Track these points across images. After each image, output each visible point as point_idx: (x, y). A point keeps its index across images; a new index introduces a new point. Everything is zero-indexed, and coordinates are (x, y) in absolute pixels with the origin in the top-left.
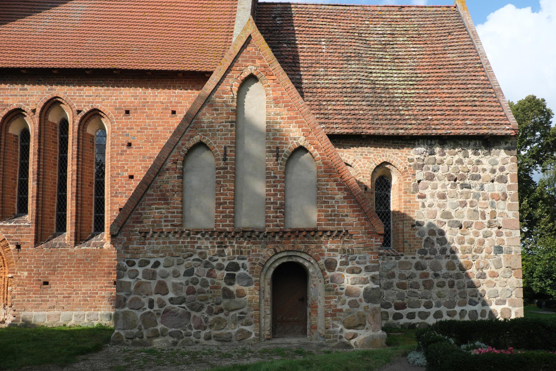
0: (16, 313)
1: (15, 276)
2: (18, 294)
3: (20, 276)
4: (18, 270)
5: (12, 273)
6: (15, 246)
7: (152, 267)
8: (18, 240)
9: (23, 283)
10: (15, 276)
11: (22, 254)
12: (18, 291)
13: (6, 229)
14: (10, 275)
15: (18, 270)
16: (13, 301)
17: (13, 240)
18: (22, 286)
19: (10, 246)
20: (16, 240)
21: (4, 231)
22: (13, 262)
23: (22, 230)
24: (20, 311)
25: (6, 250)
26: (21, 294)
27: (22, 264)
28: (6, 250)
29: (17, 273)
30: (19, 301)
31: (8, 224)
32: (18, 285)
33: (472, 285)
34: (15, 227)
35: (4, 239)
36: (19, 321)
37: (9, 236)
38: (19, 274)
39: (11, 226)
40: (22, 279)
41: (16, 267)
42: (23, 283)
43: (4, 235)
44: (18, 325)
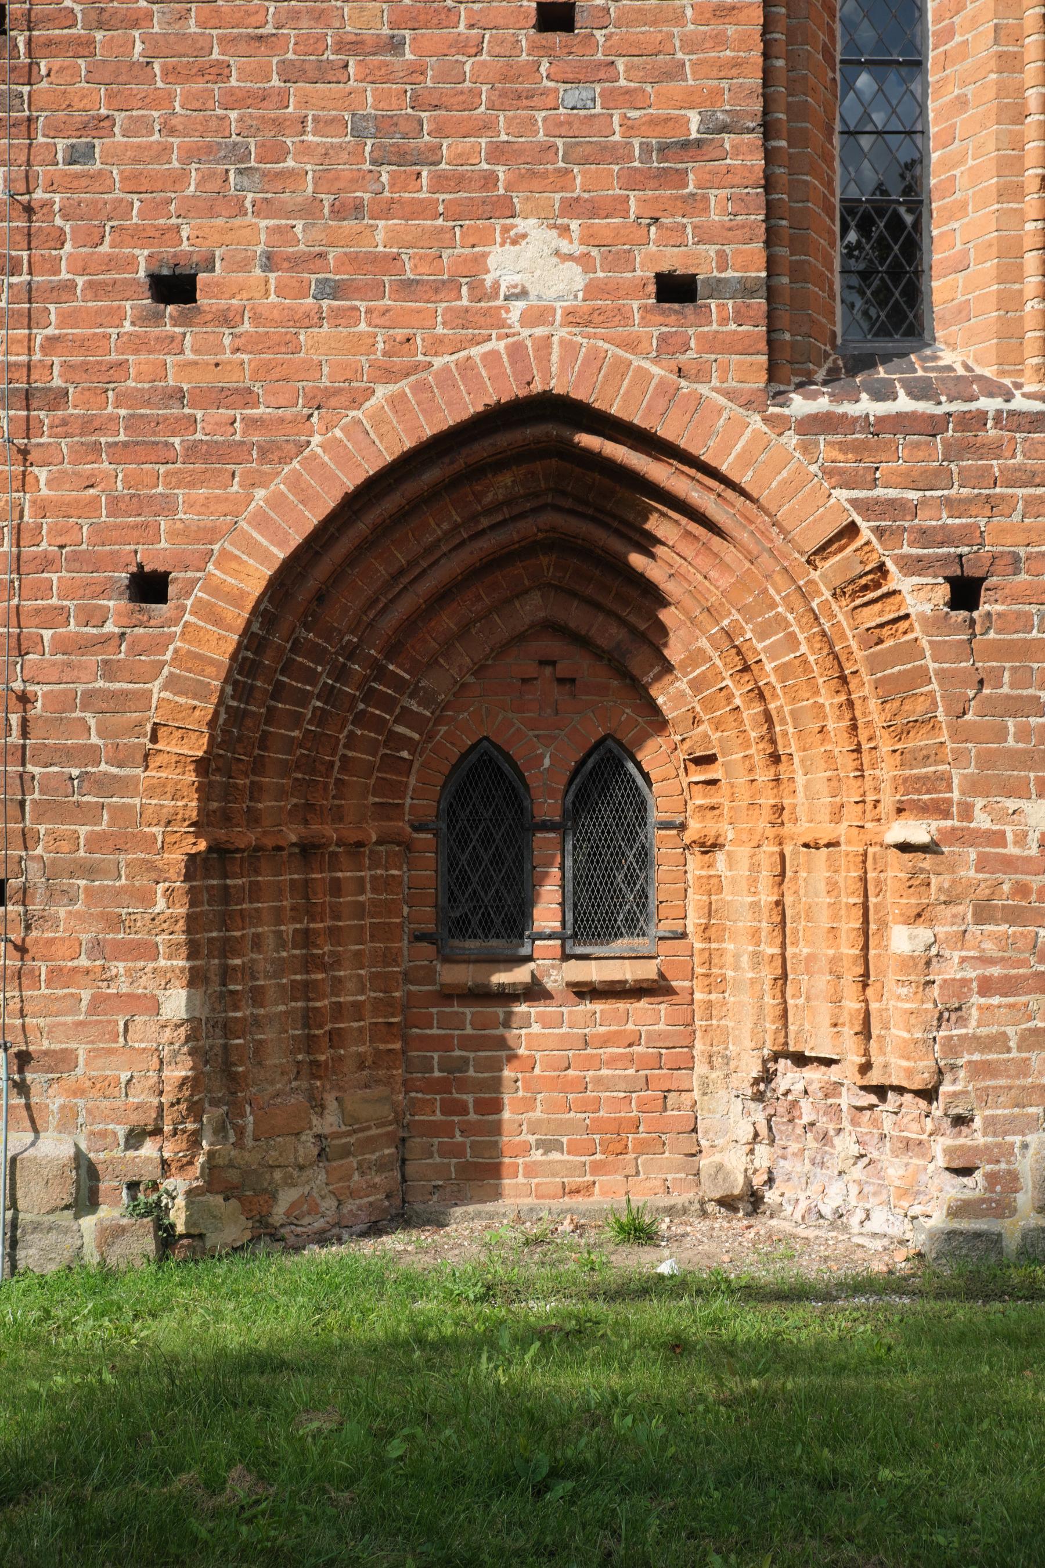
0: (977, 1136)
1: (956, 836)
2: (986, 987)
3: (998, 838)
4: (974, 787)
5: (925, 810)
6: (944, 592)
7: (848, 500)
8: (965, 536)
9: (1022, 890)
10: (956, 836)
11: (1004, 651)
12: (986, 960)
13: (858, 448)
14: (917, 831)
15: (974, 787)
16: (952, 1047)
17: (924, 537)
18: (1013, 916)
19: (897, 580)
20: (947, 537)
21: (847, 462)
22: (929, 722)
23: (996, 450)
24: (1010, 1126)
25: (871, 617)
26: (1008, 986)
27: (1001, 735)
28: (871, 617)
29: (967, 812)
30: (999, 1042)
31: (866, 406)
32: (983, 914)
33: (188, 1209)
34: (933, 426)
35: (851, 530)
36: (1003, 1208)
37: (895, 507)
38: (982, 821)
39: (900, 423)
40: (1009, 864)
41: (959, 757)
42: (1022, 890)
43: (842, 495)
44: (1012, 1243)
